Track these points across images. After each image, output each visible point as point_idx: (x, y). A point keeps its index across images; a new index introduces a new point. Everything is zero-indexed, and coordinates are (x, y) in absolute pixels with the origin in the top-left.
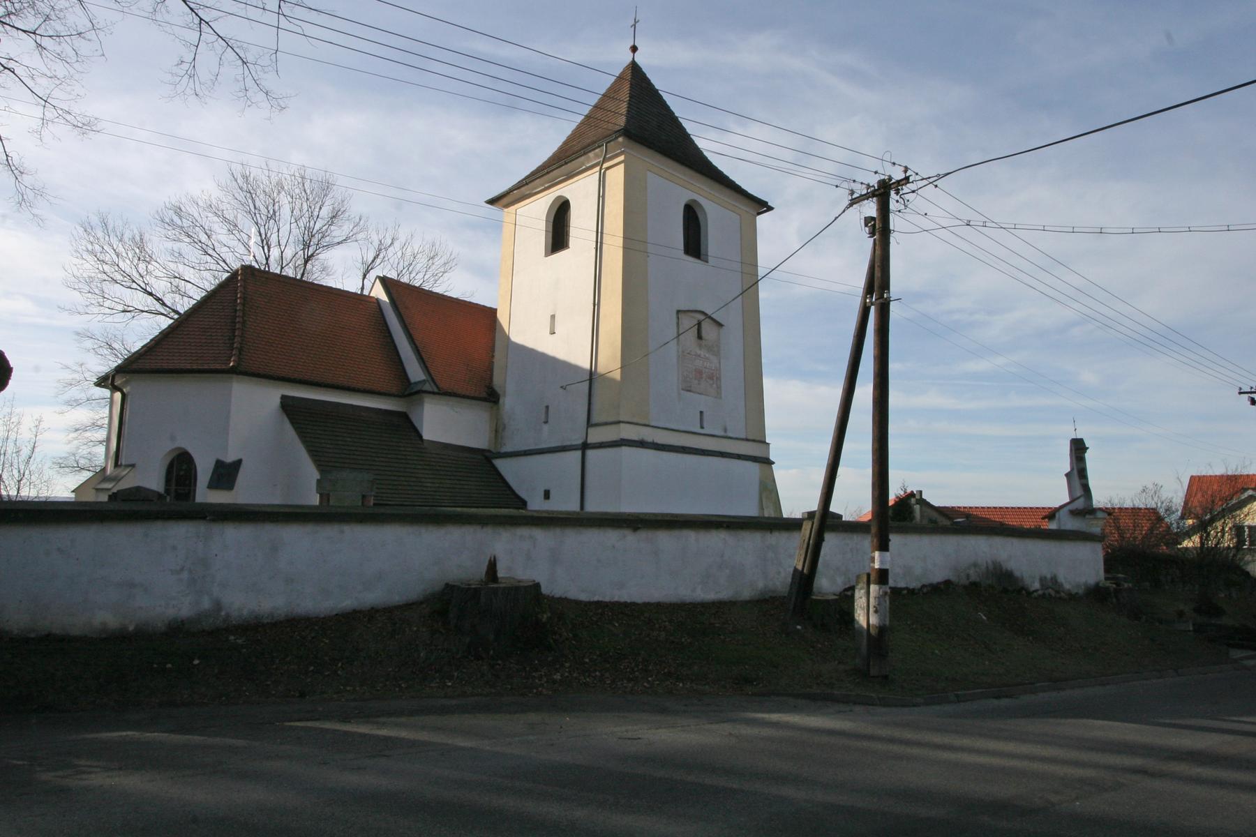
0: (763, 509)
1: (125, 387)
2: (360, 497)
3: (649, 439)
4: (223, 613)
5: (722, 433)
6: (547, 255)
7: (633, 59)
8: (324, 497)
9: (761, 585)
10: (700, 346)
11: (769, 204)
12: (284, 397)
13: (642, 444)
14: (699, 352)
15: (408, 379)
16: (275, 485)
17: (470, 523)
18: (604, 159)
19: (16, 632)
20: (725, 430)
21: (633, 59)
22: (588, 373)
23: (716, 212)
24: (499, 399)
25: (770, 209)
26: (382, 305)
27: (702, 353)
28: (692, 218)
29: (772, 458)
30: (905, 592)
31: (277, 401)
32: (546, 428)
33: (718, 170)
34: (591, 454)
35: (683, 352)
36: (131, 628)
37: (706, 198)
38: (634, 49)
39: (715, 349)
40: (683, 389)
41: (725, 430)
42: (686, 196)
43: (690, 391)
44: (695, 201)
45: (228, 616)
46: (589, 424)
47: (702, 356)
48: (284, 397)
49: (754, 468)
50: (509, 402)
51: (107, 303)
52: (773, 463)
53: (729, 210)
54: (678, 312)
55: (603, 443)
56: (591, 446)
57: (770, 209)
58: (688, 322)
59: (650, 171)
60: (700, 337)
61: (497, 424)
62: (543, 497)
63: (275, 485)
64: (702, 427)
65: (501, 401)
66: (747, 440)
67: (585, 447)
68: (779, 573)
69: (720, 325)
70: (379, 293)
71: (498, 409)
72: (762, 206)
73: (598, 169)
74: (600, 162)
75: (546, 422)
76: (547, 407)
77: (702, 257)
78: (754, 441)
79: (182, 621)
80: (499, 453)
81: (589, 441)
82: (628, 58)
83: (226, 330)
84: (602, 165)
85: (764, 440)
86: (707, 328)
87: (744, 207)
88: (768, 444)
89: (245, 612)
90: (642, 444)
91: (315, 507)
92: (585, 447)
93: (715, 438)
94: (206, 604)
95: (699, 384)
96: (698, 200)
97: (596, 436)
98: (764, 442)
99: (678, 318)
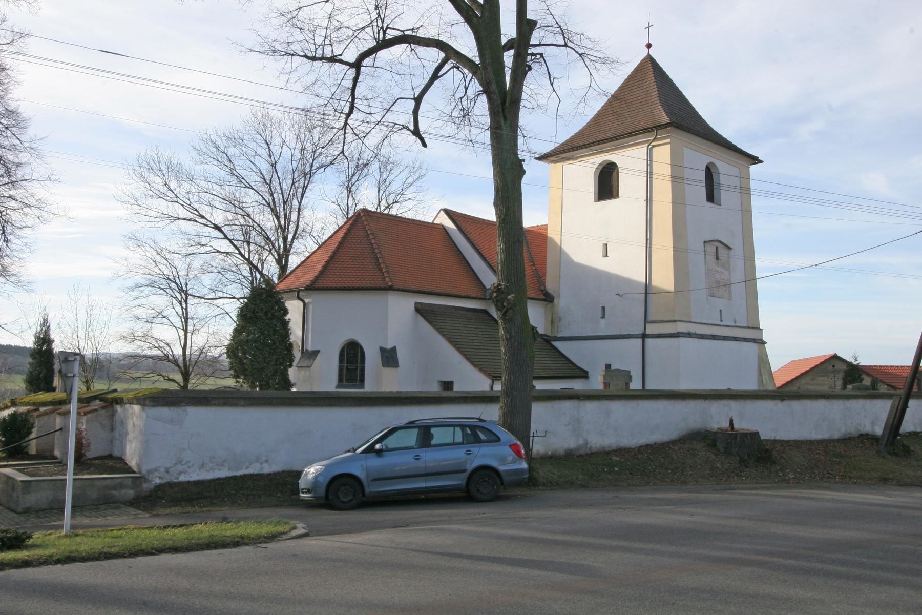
0: (762, 376)
1: (306, 298)
2: (625, 384)
3: (693, 331)
4: (589, 446)
5: (733, 324)
6: (595, 201)
7: (649, 53)
8: (606, 385)
9: (843, 430)
10: (718, 264)
11: (759, 159)
12: (416, 303)
13: (689, 335)
14: (717, 269)
15: (484, 287)
16: (414, 363)
17: (700, 398)
18: (654, 139)
19: (607, 450)
20: (735, 322)
21: (649, 53)
22: (644, 286)
23: (726, 168)
24: (553, 300)
25: (761, 162)
26: (445, 227)
27: (719, 269)
28: (710, 173)
29: (764, 339)
30: (912, 433)
31: (413, 307)
32: (603, 321)
33: (732, 144)
34: (640, 341)
35: (708, 270)
36: (549, 453)
37: (719, 160)
38: (649, 46)
39: (727, 266)
40: (709, 296)
41: (735, 322)
42: (704, 162)
43: (713, 296)
44: (712, 163)
45: (591, 447)
46: (646, 321)
47: (719, 271)
48: (416, 303)
49: (754, 347)
50: (562, 302)
51: (144, 211)
52: (766, 343)
53: (721, 161)
54: (705, 242)
55: (661, 334)
56: (650, 336)
57: (761, 162)
58: (711, 249)
59: (687, 147)
60: (717, 258)
61: (552, 317)
62: (383, 346)
63: (414, 363)
64: (721, 321)
65: (555, 301)
66: (749, 328)
67: (644, 336)
68: (852, 423)
69: (729, 248)
70: (449, 224)
71: (553, 306)
72: (755, 160)
73: (647, 145)
74: (650, 140)
75: (603, 317)
76: (603, 308)
77: (715, 201)
78: (753, 328)
79: (571, 450)
80: (556, 337)
81: (647, 332)
82: (644, 53)
83: (370, 259)
84: (650, 143)
85: (758, 326)
86: (722, 250)
87: (742, 161)
88: (762, 330)
89: (598, 445)
90: (689, 335)
91: (601, 390)
92: (644, 336)
93: (730, 328)
94: (581, 442)
95: (718, 291)
96: (714, 162)
97: (651, 329)
98: (758, 328)
99: (705, 247)
